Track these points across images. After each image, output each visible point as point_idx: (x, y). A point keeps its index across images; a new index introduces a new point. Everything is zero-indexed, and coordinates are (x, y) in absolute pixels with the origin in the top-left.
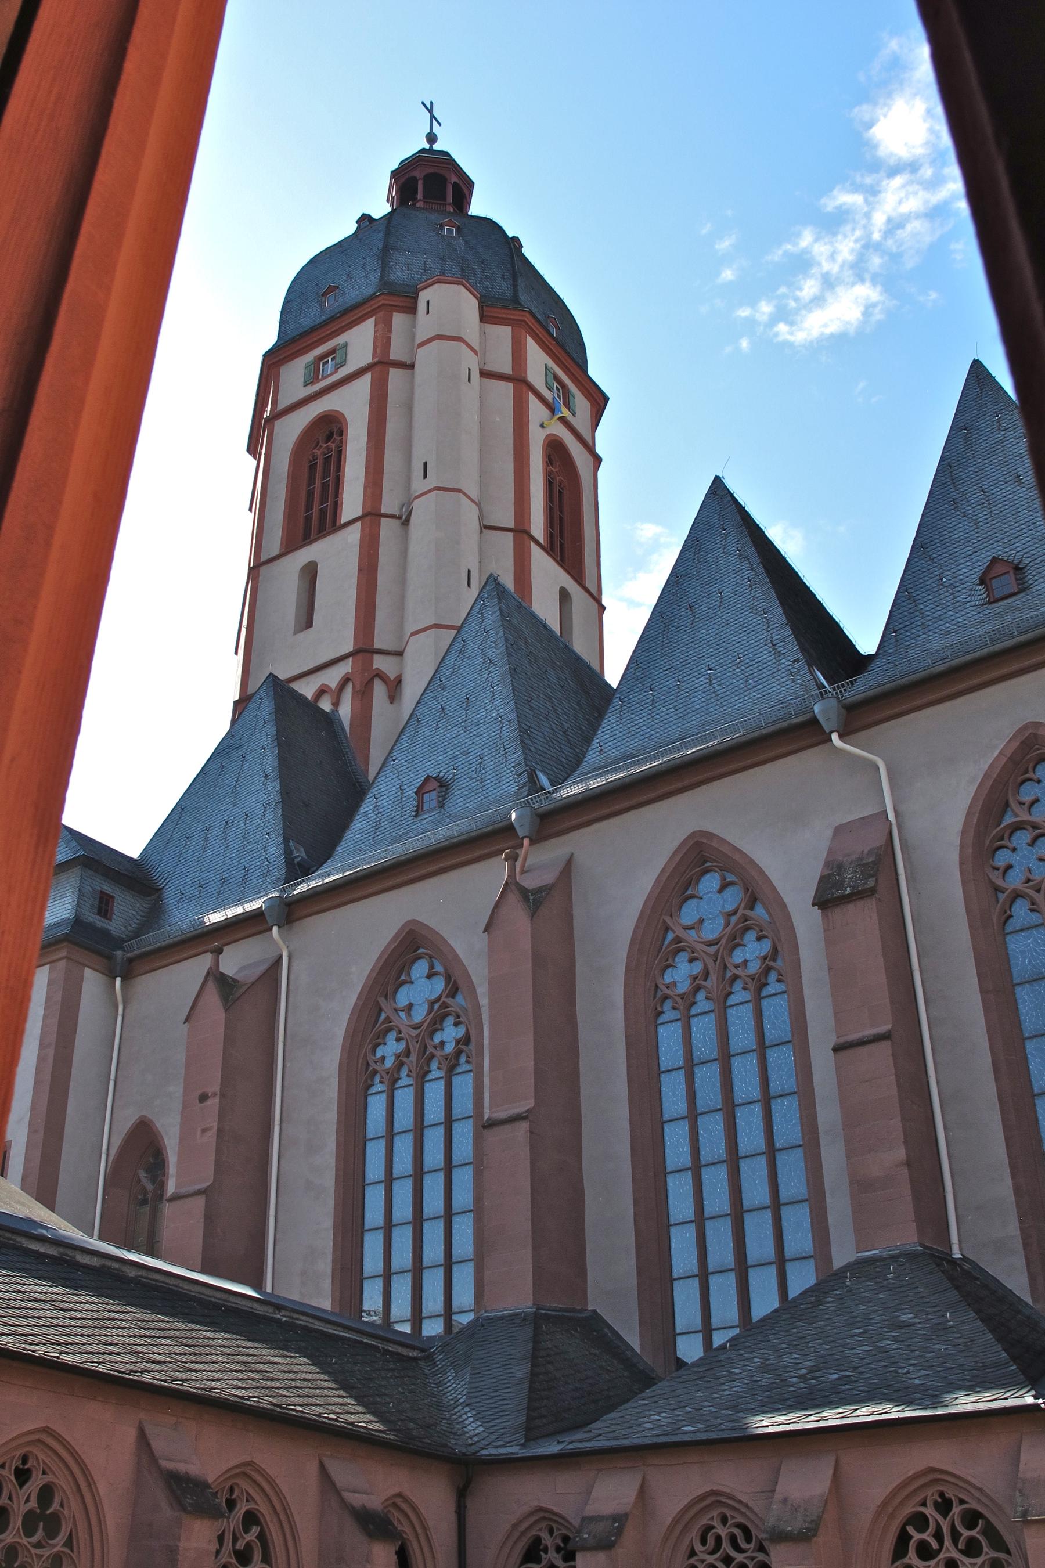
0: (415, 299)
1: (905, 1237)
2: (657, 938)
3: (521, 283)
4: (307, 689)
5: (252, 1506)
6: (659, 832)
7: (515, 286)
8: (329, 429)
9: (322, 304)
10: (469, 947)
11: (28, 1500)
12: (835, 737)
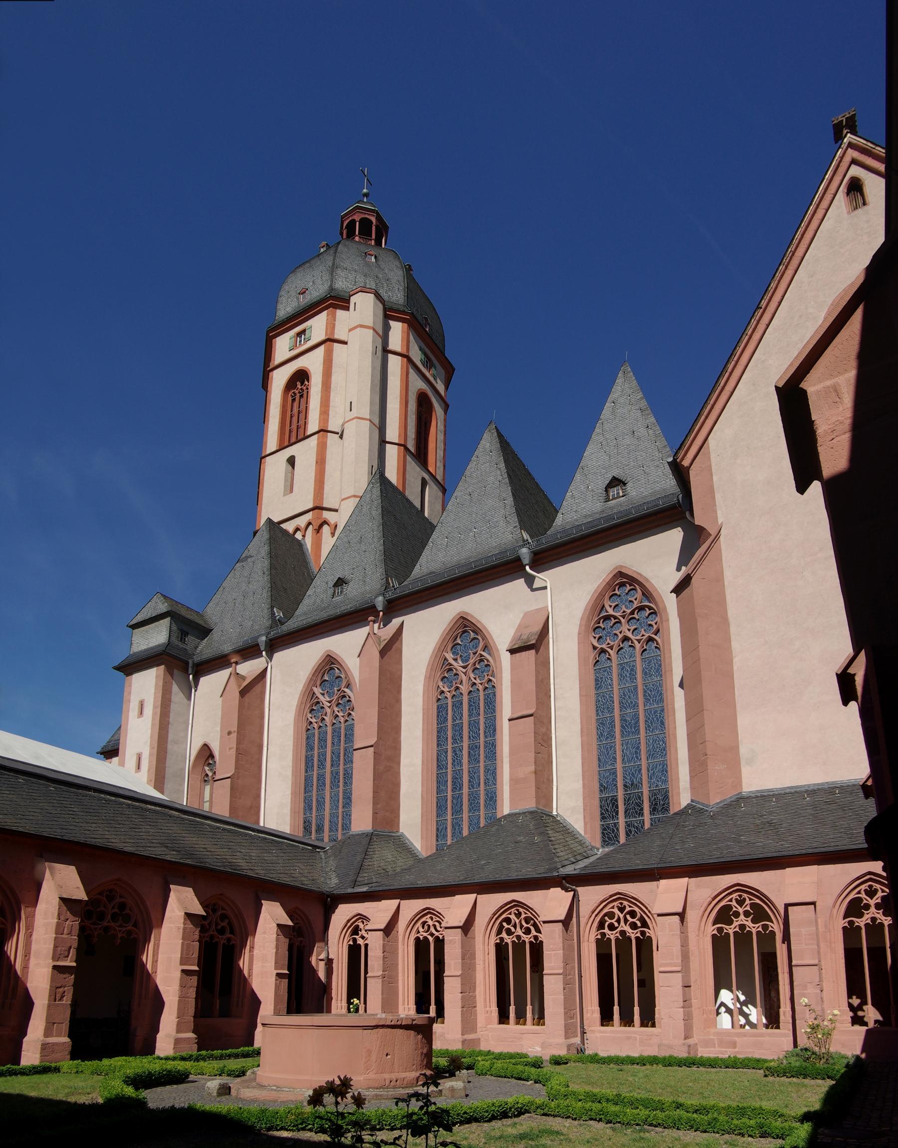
0: (348, 301)
1: (530, 804)
4: (289, 527)
5: (122, 900)
8: (301, 376)
9: (298, 299)
10: (352, 664)
11: (113, 908)
12: (527, 568)
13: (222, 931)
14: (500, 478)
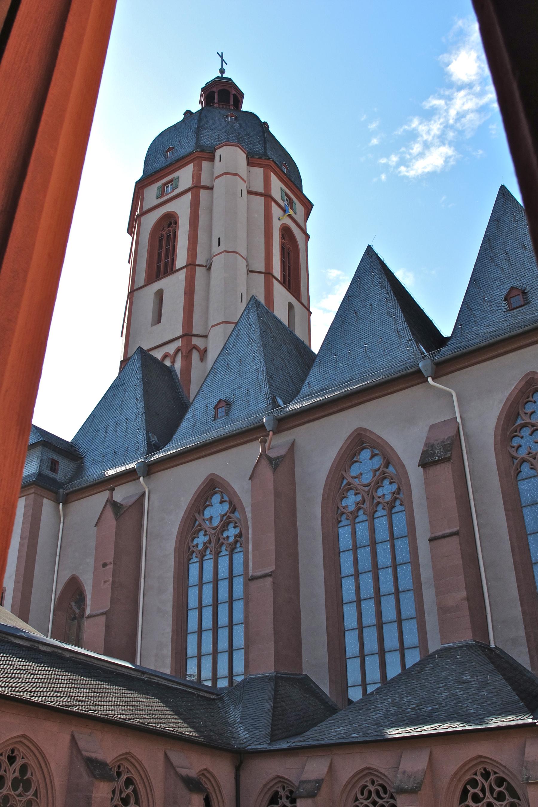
0: (214, 154)
1: (466, 636)
2: (338, 483)
3: (268, 146)
4: (158, 355)
6: (339, 428)
7: (265, 147)
9: (166, 157)
10: (241, 487)
11: (14, 772)
12: (430, 379)
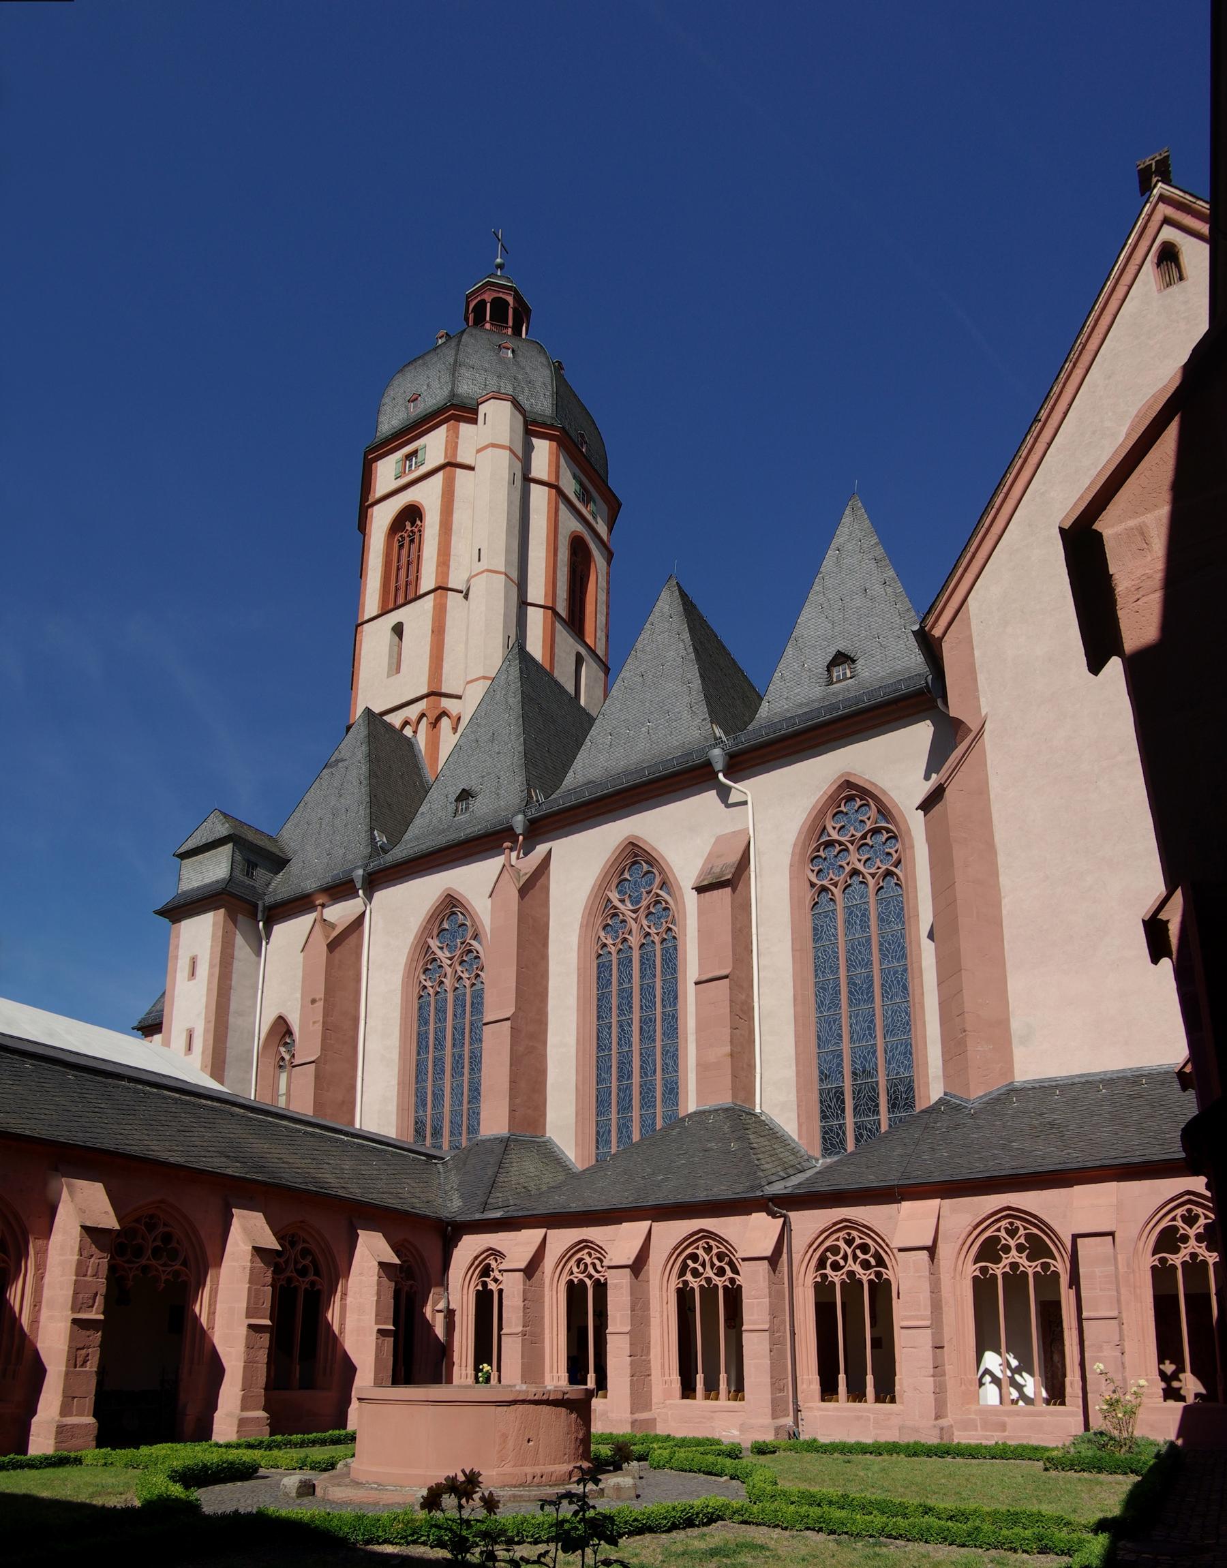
0: (476, 412)
1: (724, 1099)
4: (395, 720)
5: (167, 1229)
8: (412, 514)
9: (407, 408)
10: (481, 906)
11: (154, 1240)
12: (721, 776)
13: (303, 1272)
14: (683, 653)
